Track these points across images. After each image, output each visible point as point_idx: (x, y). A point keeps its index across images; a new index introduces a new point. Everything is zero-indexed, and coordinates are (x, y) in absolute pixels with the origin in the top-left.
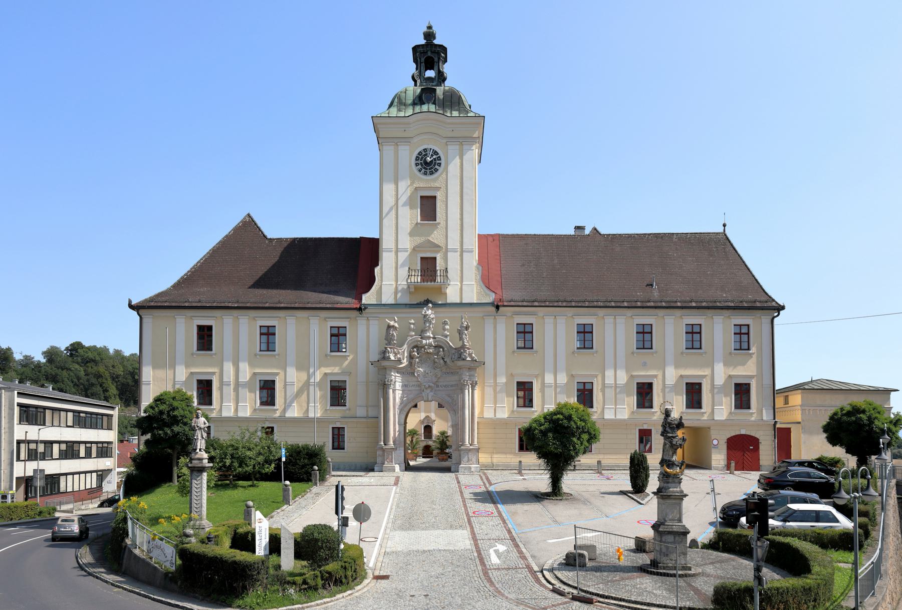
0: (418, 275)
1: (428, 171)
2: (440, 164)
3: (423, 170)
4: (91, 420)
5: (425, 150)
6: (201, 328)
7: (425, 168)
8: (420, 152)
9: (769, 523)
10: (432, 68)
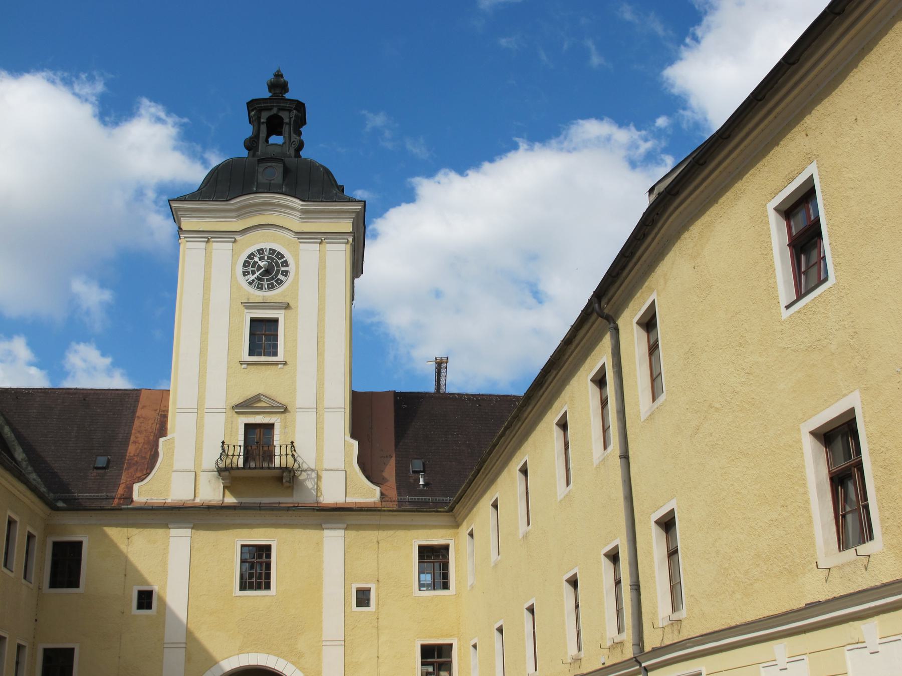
0: (233, 455)
1: (282, 269)
2: (262, 288)
4: (200, 427)
10: (280, 133)
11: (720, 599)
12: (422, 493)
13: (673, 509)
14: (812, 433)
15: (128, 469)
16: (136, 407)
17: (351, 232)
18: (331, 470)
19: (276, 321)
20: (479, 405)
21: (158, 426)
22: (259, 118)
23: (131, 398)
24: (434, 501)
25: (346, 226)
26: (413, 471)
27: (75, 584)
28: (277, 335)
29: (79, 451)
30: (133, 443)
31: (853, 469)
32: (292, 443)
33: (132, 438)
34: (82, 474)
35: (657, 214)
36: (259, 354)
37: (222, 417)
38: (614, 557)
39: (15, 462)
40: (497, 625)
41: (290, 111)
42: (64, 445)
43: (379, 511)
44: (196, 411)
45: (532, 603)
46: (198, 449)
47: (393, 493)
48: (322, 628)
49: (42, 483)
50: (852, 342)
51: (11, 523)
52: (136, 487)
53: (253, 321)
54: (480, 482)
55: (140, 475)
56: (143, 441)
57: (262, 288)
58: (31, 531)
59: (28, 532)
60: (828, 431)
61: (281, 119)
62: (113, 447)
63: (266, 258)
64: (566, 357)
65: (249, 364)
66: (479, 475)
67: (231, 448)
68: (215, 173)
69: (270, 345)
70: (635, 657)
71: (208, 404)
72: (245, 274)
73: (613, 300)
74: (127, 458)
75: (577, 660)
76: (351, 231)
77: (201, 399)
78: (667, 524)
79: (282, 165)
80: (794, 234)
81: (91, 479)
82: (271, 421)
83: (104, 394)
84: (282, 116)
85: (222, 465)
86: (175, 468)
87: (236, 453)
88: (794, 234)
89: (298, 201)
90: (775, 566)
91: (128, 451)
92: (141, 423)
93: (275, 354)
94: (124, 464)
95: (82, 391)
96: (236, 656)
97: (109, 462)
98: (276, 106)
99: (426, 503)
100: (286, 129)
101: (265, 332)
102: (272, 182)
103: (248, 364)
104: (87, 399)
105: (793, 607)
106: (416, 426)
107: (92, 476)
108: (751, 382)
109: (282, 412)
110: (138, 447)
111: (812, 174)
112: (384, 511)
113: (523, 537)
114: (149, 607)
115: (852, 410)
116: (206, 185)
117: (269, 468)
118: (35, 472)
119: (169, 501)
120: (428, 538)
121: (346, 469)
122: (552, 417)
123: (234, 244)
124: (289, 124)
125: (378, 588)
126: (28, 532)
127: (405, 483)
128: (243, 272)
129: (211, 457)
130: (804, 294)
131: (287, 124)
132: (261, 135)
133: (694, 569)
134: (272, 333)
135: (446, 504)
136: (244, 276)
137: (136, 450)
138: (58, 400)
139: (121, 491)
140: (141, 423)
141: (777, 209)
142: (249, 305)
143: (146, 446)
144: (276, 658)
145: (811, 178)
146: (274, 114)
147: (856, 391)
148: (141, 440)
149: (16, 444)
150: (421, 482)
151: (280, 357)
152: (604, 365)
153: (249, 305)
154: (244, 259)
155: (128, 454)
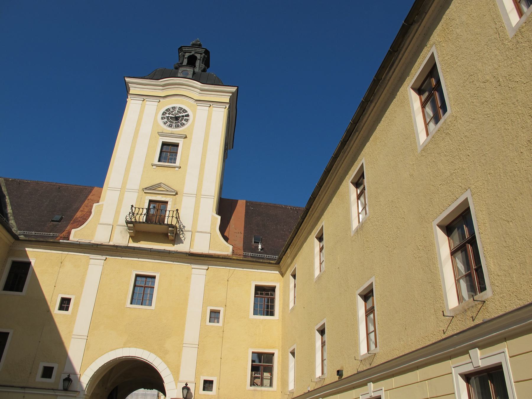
0: (138, 214)
2: (171, 127)
3: (169, 123)
5: (174, 108)
7: (170, 122)
15: (73, 224)
16: (89, 195)
18: (201, 232)
19: (176, 145)
20: (297, 212)
22: (184, 56)
23: (87, 190)
26: (254, 242)
29: (46, 212)
32: (177, 210)
33: (81, 209)
34: (43, 224)
37: (136, 195)
41: (201, 54)
42: (38, 208)
43: (231, 259)
44: (120, 190)
45: (293, 348)
48: (184, 335)
49: (16, 226)
52: (73, 231)
53: (164, 144)
57: (171, 127)
62: (67, 212)
67: (137, 209)
68: (153, 72)
69: (172, 158)
71: (128, 186)
72: (162, 118)
74: (74, 218)
77: (124, 183)
78: (367, 295)
81: (48, 227)
82: (166, 200)
83: (72, 187)
84: (197, 56)
85: (129, 219)
86: (100, 222)
87: (140, 213)
89: (199, 83)
91: (76, 215)
93: (175, 163)
96: (122, 349)
97: (62, 218)
100: (198, 63)
103: (157, 166)
104: (61, 188)
106: (258, 219)
107: (49, 225)
109: (174, 195)
110: (83, 213)
112: (234, 259)
120: (262, 281)
121: (211, 233)
123: (159, 103)
124: (200, 60)
127: (248, 247)
128: (162, 117)
129: (124, 214)
131: (198, 59)
136: (162, 119)
138: (43, 187)
140: (89, 202)
142: (162, 134)
143: (88, 214)
146: (193, 55)
149: (9, 205)
151: (178, 164)
153: (162, 134)
154: (164, 111)
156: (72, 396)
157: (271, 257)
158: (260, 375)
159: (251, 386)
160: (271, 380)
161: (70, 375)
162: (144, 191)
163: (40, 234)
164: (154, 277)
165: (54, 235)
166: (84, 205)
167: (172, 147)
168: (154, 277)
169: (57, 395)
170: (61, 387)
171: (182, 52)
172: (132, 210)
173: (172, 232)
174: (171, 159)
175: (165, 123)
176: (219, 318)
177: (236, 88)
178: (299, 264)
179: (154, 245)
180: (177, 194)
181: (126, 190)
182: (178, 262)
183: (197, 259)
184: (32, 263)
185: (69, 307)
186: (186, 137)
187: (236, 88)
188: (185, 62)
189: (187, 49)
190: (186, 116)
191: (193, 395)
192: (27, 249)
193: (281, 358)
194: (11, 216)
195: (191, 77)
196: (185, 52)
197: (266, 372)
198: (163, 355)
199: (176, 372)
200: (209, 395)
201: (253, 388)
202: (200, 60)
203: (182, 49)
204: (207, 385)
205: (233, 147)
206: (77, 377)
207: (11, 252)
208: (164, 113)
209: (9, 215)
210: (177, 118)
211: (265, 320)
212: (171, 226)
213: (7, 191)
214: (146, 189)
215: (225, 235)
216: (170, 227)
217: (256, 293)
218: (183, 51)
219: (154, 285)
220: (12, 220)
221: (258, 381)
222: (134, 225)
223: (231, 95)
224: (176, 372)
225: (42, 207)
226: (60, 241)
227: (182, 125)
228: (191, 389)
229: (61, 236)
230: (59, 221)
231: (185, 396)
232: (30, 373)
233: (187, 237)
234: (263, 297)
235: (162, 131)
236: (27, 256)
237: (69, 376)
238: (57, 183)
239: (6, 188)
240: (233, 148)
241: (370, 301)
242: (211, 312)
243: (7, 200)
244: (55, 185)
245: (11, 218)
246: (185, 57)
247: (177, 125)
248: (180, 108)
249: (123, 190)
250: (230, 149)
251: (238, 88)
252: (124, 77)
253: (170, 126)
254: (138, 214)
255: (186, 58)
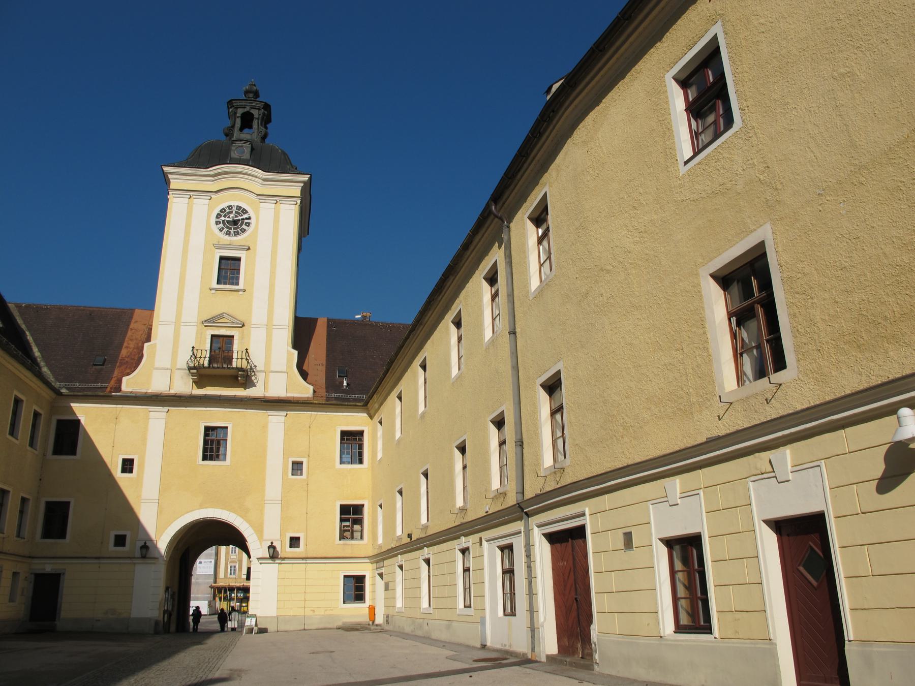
0: (201, 357)
2: (229, 234)
3: (226, 230)
5: (230, 207)
6: (625, 534)
7: (227, 227)
8: (223, 209)
9: (222, 547)
11: (606, 444)
12: (345, 392)
13: (560, 370)
14: (712, 276)
15: (119, 367)
16: (130, 322)
17: (299, 197)
19: (238, 259)
20: (391, 331)
21: (146, 336)
22: (236, 113)
24: (354, 398)
25: (296, 191)
26: (339, 376)
27: (73, 452)
28: (239, 270)
30: (125, 348)
31: (756, 306)
32: (247, 349)
33: (125, 344)
35: (553, 111)
36: (225, 283)
37: (195, 329)
38: (499, 423)
39: (31, 361)
40: (398, 489)
43: (311, 403)
44: (174, 323)
46: (175, 353)
47: (323, 392)
50: (762, 177)
51: (18, 402)
52: (125, 379)
53: (222, 258)
54: (388, 380)
55: (129, 371)
56: (133, 346)
58: (36, 409)
59: (35, 410)
60: (727, 274)
61: (252, 115)
63: (234, 212)
64: (463, 262)
65: (217, 290)
66: (388, 374)
67: (199, 352)
70: (518, 504)
72: (217, 223)
73: (505, 206)
74: (120, 358)
75: (463, 510)
76: (300, 196)
78: (552, 386)
79: (250, 146)
80: (691, 100)
82: (232, 334)
84: (253, 113)
85: (192, 365)
88: (691, 100)
89: (260, 171)
90: (667, 408)
92: (133, 333)
93: (237, 284)
94: (117, 363)
95: (89, 309)
98: (249, 105)
99: (348, 400)
100: (255, 123)
101: (231, 267)
102: (242, 157)
104: (92, 314)
105: (692, 443)
108: (646, 239)
111: (716, 34)
112: (315, 404)
113: (421, 417)
114: (131, 471)
115: (762, 244)
116: (191, 157)
117: (228, 368)
118: (47, 367)
119: (150, 391)
122: (450, 316)
124: (258, 119)
125: (309, 462)
126: (35, 410)
127: (332, 385)
129: (184, 358)
130: (701, 149)
132: (236, 126)
133: (579, 420)
134: (236, 268)
135: (362, 400)
137: (128, 353)
139: (112, 383)
140: (133, 333)
141: (675, 79)
142: (218, 246)
143: (135, 351)
144: (229, 512)
145: (715, 38)
146: (248, 111)
147: (767, 224)
148: (132, 346)
150: (345, 384)
151: (241, 286)
152: (495, 263)
153: (218, 246)
155: (121, 356)
156: (151, 563)
157: (358, 397)
158: (350, 528)
159: (340, 540)
160: (362, 532)
161: (147, 542)
162: (205, 324)
163: (85, 385)
164: (226, 428)
165: (102, 385)
166: (128, 338)
167: (232, 262)
168: (226, 428)
169: (135, 564)
170: (138, 553)
171: (233, 108)
172: (193, 352)
173: (242, 376)
174: (232, 278)
175: (221, 230)
176: (301, 470)
177: (309, 176)
178: (383, 412)
179: (222, 390)
180: (243, 325)
181: (182, 324)
182: (252, 409)
183: (274, 405)
184: (81, 421)
185: (133, 468)
186: (249, 249)
187: (309, 176)
188: (238, 122)
189: (240, 102)
190: (246, 219)
191: (280, 553)
192: (72, 405)
193: (371, 509)
194: (41, 361)
195: (246, 155)
196: (237, 108)
197: (355, 524)
198: (243, 513)
199: (259, 531)
200: (296, 552)
201: (342, 542)
202: (258, 119)
203: (232, 103)
204: (294, 541)
205: (308, 232)
206: (153, 543)
207: (53, 408)
208: (218, 216)
209: (38, 359)
210: (235, 222)
211: (353, 469)
212: (241, 369)
213: (25, 323)
214: (205, 321)
215: (304, 368)
216: (240, 371)
217: (342, 439)
218: (233, 106)
219: (227, 437)
220: (44, 367)
221: (348, 534)
222: (197, 371)
223: (302, 184)
224: (259, 531)
225: (76, 345)
226: (113, 394)
227: (243, 232)
228: (276, 547)
229: (111, 386)
230: (103, 365)
231: (271, 555)
232: (102, 543)
233: (259, 379)
234: (350, 443)
235: (219, 242)
236: (74, 413)
237: (145, 543)
238: (85, 307)
239: (23, 319)
240: (308, 234)
241: (556, 395)
242: (292, 463)
243: (28, 338)
244: (84, 310)
245: (42, 364)
246: (238, 115)
247: (236, 232)
248: (239, 208)
249: (177, 324)
250: (304, 237)
251: (311, 177)
252: (162, 166)
253: (228, 234)
254: (201, 357)
255: (238, 117)
